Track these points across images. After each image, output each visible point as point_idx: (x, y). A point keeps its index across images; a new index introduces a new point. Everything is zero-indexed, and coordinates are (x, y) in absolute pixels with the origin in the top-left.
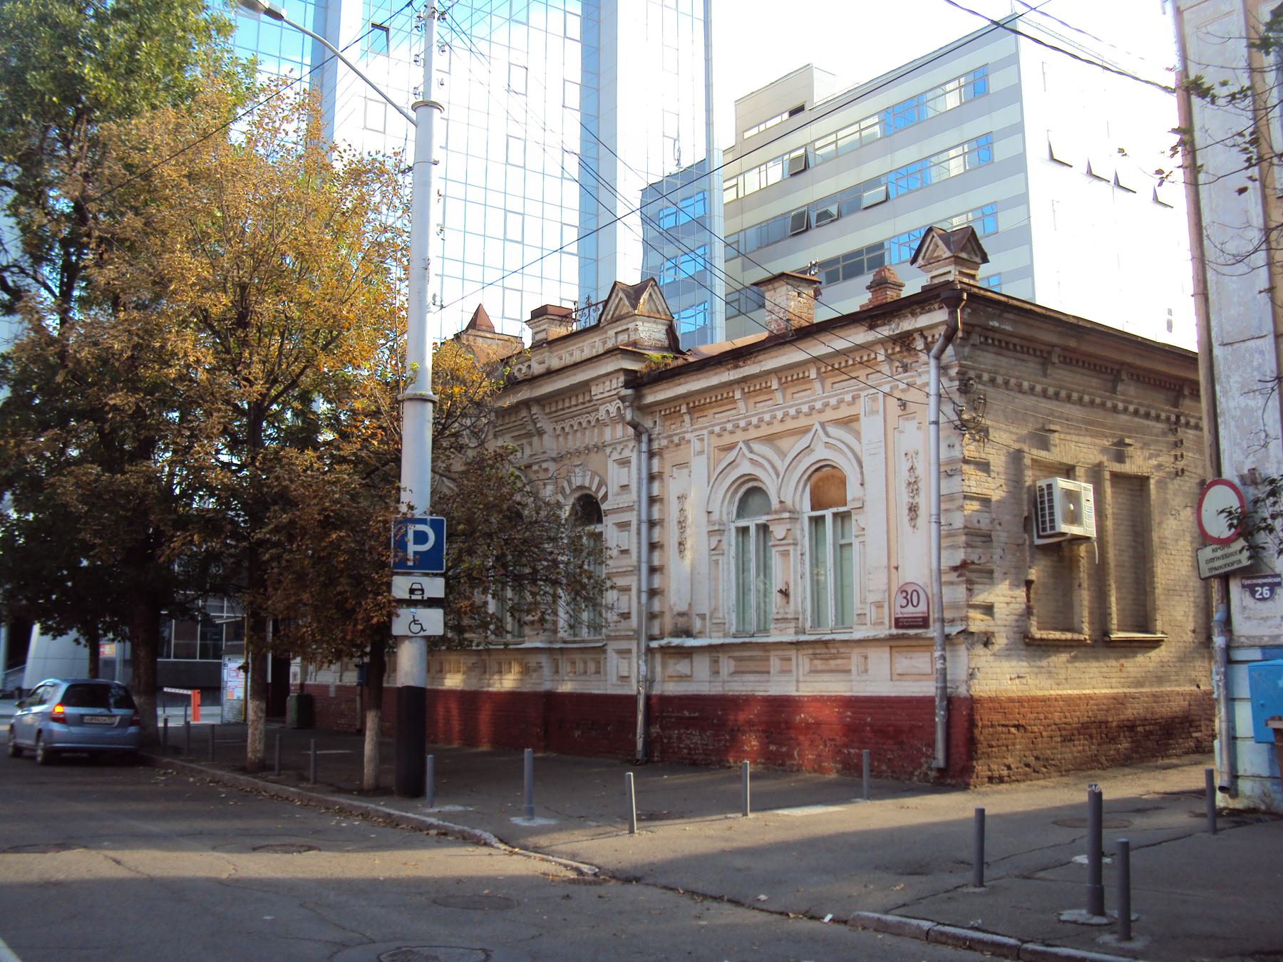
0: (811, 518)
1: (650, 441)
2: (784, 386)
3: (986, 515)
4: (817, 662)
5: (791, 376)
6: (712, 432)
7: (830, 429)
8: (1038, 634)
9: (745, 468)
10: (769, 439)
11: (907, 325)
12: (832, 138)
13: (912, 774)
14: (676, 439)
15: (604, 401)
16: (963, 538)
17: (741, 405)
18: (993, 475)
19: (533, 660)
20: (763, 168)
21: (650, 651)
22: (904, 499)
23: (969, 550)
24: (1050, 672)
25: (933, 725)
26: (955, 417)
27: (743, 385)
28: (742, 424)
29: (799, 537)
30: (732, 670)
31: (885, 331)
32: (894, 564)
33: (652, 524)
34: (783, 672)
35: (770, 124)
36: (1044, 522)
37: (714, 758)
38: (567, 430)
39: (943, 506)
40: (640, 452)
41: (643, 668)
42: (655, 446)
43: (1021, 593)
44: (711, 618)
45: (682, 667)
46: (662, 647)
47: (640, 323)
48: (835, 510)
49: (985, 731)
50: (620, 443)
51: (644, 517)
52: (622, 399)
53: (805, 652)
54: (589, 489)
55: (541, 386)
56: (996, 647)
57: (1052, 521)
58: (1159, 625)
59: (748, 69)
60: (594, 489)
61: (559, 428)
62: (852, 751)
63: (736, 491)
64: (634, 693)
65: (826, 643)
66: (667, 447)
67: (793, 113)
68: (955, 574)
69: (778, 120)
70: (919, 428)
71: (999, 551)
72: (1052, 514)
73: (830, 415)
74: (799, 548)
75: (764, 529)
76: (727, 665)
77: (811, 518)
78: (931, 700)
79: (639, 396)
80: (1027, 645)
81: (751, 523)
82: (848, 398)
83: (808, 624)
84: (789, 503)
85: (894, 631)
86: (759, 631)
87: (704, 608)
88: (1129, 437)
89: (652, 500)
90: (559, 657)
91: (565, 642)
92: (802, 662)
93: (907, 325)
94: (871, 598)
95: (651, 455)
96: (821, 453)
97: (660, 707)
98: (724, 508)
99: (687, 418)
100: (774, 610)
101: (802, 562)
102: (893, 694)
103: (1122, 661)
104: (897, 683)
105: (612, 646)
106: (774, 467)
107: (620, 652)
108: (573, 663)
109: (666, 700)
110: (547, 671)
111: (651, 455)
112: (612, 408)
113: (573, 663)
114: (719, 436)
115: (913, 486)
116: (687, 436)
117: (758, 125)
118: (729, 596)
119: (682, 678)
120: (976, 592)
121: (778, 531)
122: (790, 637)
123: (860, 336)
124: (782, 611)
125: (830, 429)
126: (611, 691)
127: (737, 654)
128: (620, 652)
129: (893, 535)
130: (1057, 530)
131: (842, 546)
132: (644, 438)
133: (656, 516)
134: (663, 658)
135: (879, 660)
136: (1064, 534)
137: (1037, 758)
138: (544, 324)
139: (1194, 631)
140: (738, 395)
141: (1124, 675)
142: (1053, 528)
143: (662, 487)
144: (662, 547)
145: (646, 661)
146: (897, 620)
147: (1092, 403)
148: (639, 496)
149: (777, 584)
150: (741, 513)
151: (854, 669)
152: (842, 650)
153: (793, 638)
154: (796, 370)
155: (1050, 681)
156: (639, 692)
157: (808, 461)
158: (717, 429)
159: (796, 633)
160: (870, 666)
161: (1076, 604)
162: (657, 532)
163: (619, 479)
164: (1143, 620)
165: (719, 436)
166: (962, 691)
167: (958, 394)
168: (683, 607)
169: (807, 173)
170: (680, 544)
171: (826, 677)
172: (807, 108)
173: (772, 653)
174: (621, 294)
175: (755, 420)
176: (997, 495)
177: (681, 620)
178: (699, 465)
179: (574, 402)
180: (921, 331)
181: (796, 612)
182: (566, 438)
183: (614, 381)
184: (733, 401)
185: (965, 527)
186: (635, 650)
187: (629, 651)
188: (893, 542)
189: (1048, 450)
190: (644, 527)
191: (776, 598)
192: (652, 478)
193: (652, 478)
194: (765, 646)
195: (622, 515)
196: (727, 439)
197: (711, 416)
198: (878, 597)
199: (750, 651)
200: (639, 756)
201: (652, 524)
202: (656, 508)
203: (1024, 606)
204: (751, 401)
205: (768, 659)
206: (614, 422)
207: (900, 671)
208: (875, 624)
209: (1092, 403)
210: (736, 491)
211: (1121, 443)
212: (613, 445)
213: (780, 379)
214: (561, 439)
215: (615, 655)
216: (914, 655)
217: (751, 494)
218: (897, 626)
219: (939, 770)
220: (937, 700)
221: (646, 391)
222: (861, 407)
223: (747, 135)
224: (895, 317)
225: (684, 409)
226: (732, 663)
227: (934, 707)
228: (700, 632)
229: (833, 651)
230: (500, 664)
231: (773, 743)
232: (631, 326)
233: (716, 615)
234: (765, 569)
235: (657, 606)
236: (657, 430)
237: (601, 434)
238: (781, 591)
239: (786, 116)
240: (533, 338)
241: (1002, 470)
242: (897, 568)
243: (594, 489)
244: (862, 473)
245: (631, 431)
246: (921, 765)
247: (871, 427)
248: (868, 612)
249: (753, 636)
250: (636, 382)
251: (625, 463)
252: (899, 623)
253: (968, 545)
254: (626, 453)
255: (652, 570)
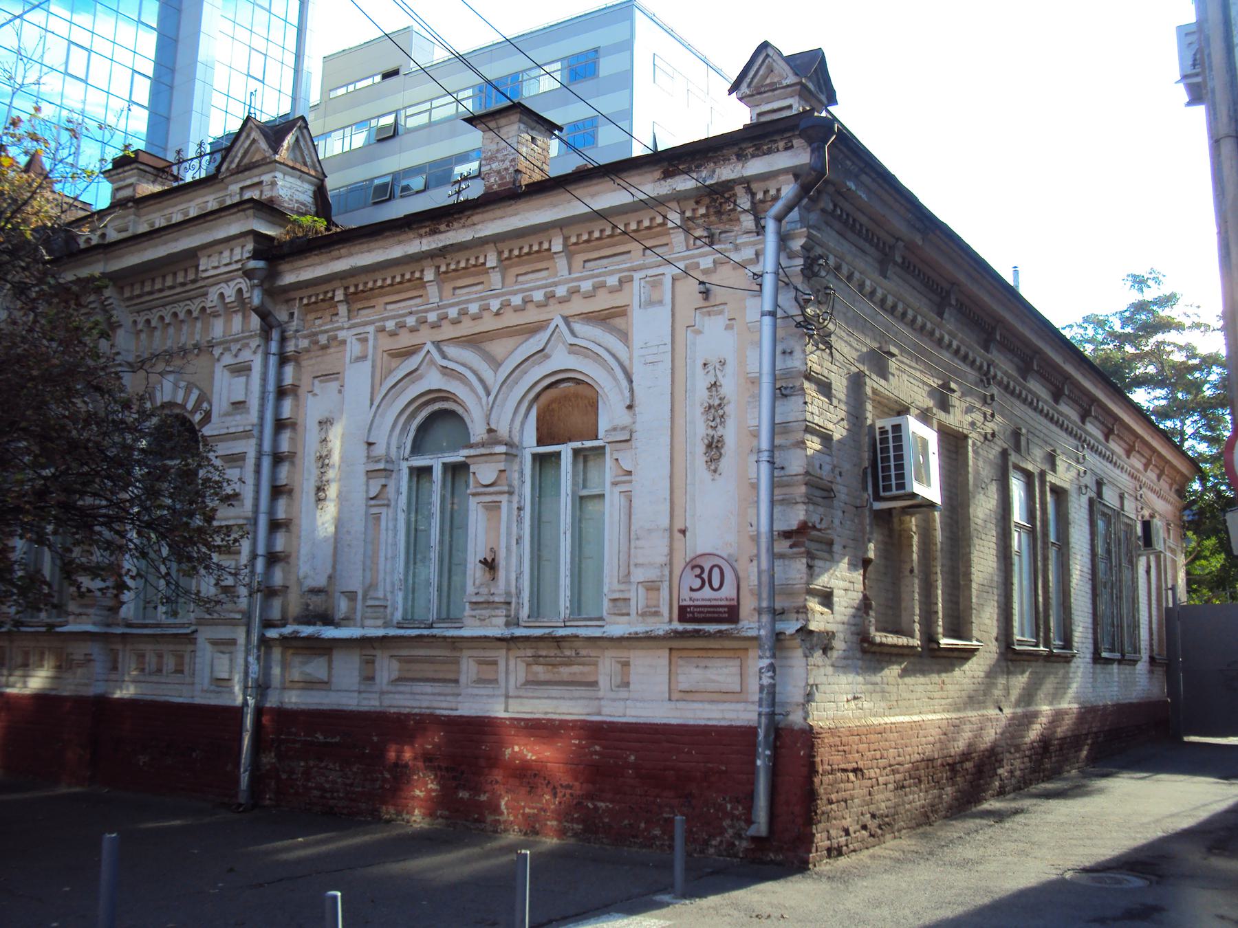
0: (536, 457)
1: (283, 340)
2: (505, 264)
3: (828, 459)
4: (538, 669)
5: (523, 249)
6: (382, 330)
7: (577, 327)
8: (879, 637)
9: (433, 380)
10: (473, 341)
11: (726, 172)
12: (427, 106)
13: (706, 843)
14: (323, 339)
15: (217, 280)
16: (803, 489)
17: (432, 291)
18: (835, 402)
19: (78, 650)
20: (348, 130)
21: (264, 642)
22: (700, 429)
23: (811, 507)
24: (883, 691)
25: (753, 770)
26: (795, 311)
27: (438, 261)
28: (432, 317)
29: (516, 483)
30: (395, 675)
31: (684, 184)
32: (679, 525)
33: (278, 459)
34: (480, 681)
35: (359, 85)
36: (887, 478)
37: (363, 806)
38: (153, 323)
39: (777, 442)
40: (267, 354)
41: (254, 668)
42: (290, 347)
43: (858, 576)
44: (365, 598)
45: (316, 668)
46: (284, 639)
47: (279, 175)
48: (578, 445)
49: (825, 779)
50: (237, 341)
51: (267, 446)
52: (248, 274)
53: (521, 653)
54: (183, 406)
55: (121, 256)
56: (835, 654)
57: (900, 476)
58: (975, 633)
59: (337, 29)
60: (190, 406)
61: (141, 320)
62: (602, 805)
63: (413, 416)
64: (239, 701)
65: (558, 641)
66: (307, 350)
67: (386, 76)
68: (787, 543)
69: (369, 82)
70: (728, 327)
71: (840, 513)
72: (900, 467)
73: (578, 306)
74: (515, 498)
75: (457, 471)
76: (387, 668)
77: (536, 457)
78: (750, 732)
79: (272, 274)
80: (864, 651)
81: (436, 463)
82: (612, 281)
83: (525, 612)
84: (503, 431)
85: (680, 627)
86: (440, 620)
87: (355, 583)
88: (956, 382)
89: (280, 425)
90: (119, 647)
91: (130, 625)
92: (514, 668)
93: (726, 172)
94: (639, 575)
95: (283, 360)
96: (561, 360)
97: (281, 727)
98: (392, 437)
99: (342, 309)
100: (470, 589)
101: (520, 521)
102: (674, 722)
103: (944, 675)
104: (681, 705)
105: (205, 634)
106: (481, 381)
107: (215, 643)
108: (141, 656)
109: (285, 716)
110: (99, 668)
111: (283, 360)
112: (230, 292)
113: (141, 656)
114: (393, 334)
115: (715, 411)
116: (342, 335)
117: (347, 85)
118: (391, 566)
119: (310, 684)
120: (817, 570)
121: (485, 473)
122: (496, 628)
123: (651, 186)
124: (484, 590)
125: (577, 327)
126: (198, 701)
127: (404, 653)
128: (215, 643)
129: (678, 482)
130: (908, 490)
131: (582, 498)
132: (275, 334)
133: (285, 447)
134: (283, 654)
135: (650, 669)
136: (914, 496)
137: (873, 816)
138: (131, 176)
139: (997, 639)
140: (429, 275)
141: (944, 694)
142: (901, 486)
143: (296, 406)
144: (290, 492)
145: (258, 658)
146: (683, 610)
147: (923, 328)
148: (262, 418)
149: (476, 549)
150: (417, 449)
151: (603, 681)
152: (583, 652)
153: (506, 632)
154: (531, 239)
155: (883, 704)
156: (245, 703)
157: (537, 372)
158: (390, 325)
159: (507, 624)
160: (633, 678)
161: (904, 596)
162: (284, 471)
163: (230, 393)
164: (959, 628)
165: (393, 334)
166: (796, 718)
167: (801, 278)
168: (321, 581)
169: (397, 139)
170: (319, 489)
171: (555, 691)
172: (402, 72)
173: (466, 653)
174: (255, 134)
175: (453, 313)
176: (839, 432)
177: (316, 600)
178: (358, 378)
179: (169, 282)
180: (747, 182)
181: (508, 594)
182: (151, 336)
183: (237, 251)
184: (422, 284)
185: (807, 473)
186: (241, 639)
187: (233, 642)
188: (678, 493)
189: (886, 379)
190: (266, 463)
191: (474, 573)
192: (281, 393)
193: (281, 393)
194: (456, 643)
195: (230, 444)
196: (405, 340)
197: (379, 308)
198: (652, 574)
199: (427, 646)
200: (242, 798)
201: (278, 459)
202: (286, 436)
203: (861, 596)
204: (448, 287)
205: (456, 662)
206: (228, 310)
207: (682, 687)
208: (644, 614)
209: (923, 328)
210: (413, 416)
211: (946, 386)
212: (226, 344)
213: (500, 253)
214: (143, 336)
215: (209, 647)
216: (709, 663)
217: (438, 420)
218: (682, 619)
219: (755, 839)
220: (761, 733)
221: (284, 267)
222: (636, 292)
223: (333, 95)
224: (709, 160)
225: (340, 295)
226: (395, 665)
227: (754, 745)
228: (346, 619)
229: (568, 653)
230: (26, 654)
231: (464, 788)
232: (266, 178)
233: (371, 594)
234: (454, 525)
235: (278, 577)
236: (294, 324)
237: (207, 329)
238: (484, 562)
239: (378, 78)
240: (113, 196)
241: (843, 397)
242: (683, 532)
243: (190, 406)
244: (632, 390)
245: (255, 321)
246: (722, 831)
247: (649, 327)
248: (632, 595)
249: (431, 627)
250: (272, 254)
251: (242, 370)
252: (685, 614)
253: (809, 500)
254: (246, 355)
255: (275, 526)
